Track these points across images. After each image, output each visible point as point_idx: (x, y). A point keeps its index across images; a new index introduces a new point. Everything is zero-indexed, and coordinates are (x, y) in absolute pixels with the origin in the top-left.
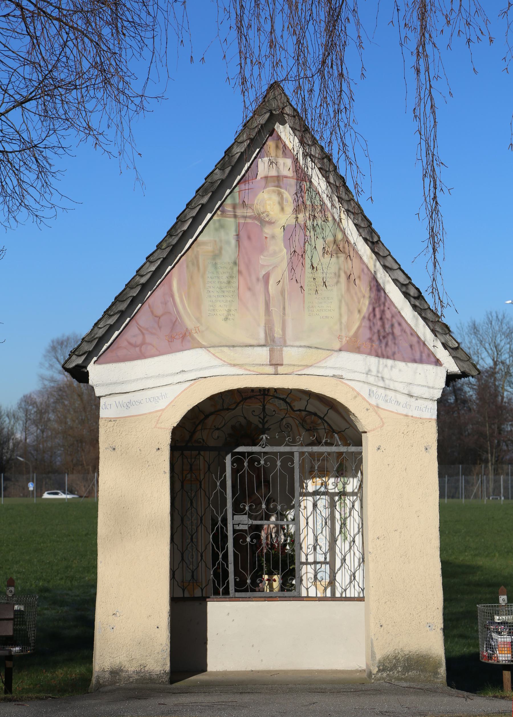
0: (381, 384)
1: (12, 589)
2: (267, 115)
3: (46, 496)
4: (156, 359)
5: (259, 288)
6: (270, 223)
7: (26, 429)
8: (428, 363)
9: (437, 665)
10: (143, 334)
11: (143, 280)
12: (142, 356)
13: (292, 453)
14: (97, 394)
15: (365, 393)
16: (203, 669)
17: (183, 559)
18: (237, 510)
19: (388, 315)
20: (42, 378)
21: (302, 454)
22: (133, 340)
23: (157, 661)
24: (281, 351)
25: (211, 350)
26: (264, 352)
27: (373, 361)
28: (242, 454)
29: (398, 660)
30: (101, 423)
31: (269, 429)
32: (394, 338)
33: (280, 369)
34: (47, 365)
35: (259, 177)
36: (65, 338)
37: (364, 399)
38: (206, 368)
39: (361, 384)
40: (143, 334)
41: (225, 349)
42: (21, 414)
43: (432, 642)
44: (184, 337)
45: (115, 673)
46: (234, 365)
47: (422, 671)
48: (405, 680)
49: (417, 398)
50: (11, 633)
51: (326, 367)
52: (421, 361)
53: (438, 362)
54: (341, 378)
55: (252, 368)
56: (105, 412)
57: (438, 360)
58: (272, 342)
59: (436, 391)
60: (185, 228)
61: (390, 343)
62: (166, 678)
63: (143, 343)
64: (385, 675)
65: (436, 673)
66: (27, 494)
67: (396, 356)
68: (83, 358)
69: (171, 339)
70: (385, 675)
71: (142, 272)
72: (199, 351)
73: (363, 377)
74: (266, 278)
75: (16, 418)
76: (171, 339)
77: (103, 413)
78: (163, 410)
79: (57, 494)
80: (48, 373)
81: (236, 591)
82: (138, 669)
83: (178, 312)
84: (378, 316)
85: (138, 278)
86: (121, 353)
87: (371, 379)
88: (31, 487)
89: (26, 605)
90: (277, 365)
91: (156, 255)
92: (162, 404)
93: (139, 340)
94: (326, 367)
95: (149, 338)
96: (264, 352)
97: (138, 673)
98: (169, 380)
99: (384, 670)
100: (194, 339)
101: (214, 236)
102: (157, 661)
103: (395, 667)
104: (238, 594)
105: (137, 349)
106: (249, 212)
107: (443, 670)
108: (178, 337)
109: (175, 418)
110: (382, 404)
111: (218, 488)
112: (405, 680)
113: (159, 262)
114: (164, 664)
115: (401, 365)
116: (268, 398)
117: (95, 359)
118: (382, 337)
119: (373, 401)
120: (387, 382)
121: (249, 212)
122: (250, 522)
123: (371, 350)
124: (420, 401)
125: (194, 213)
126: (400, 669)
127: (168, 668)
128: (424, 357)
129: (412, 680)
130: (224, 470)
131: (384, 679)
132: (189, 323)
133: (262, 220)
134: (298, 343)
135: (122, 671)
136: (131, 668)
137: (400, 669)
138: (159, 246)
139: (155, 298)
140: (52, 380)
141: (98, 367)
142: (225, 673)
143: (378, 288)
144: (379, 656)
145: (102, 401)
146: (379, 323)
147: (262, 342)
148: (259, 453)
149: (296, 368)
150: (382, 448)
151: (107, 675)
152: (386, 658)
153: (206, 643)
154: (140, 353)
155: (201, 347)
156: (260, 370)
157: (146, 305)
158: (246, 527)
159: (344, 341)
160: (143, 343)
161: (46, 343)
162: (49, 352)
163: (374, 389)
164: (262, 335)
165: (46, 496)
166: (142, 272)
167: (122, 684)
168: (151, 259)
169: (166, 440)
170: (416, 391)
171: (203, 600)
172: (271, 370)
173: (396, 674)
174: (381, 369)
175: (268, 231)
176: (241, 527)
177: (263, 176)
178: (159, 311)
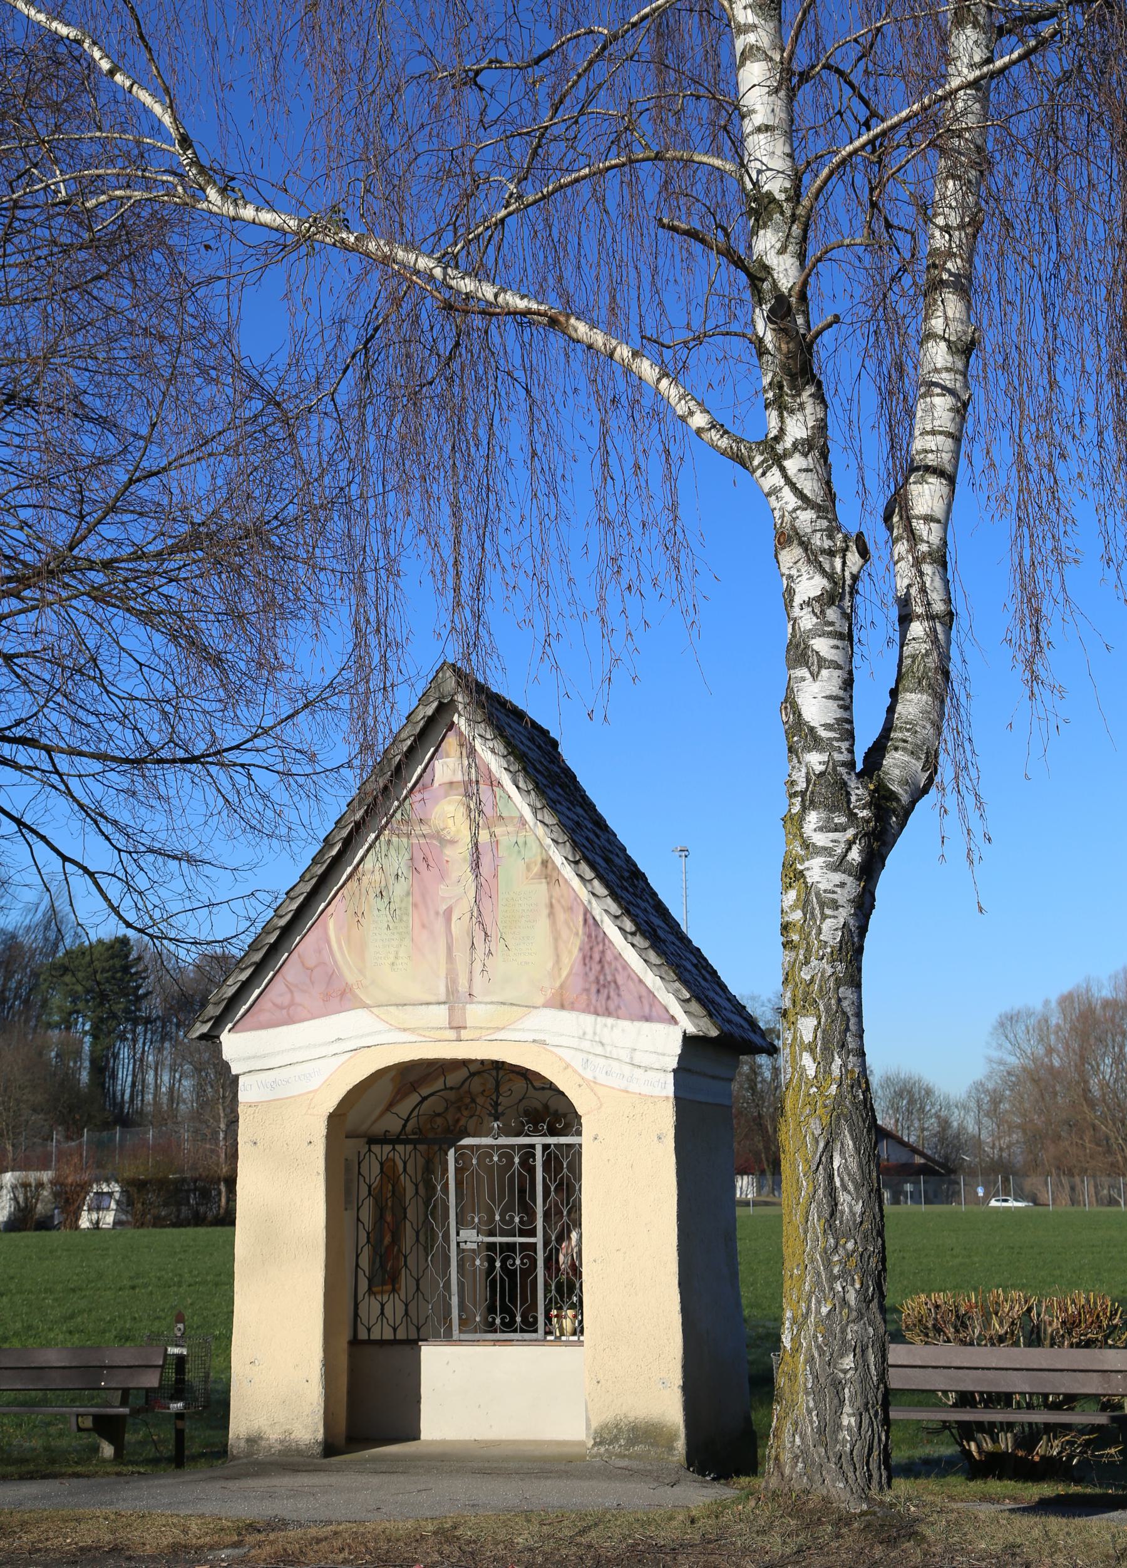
0: (599, 1050)
1: (181, 1326)
2: (435, 704)
3: (993, 1203)
4: (306, 1024)
5: (439, 925)
6: (453, 842)
7: (979, 1122)
8: (660, 1020)
9: (673, 1438)
10: (291, 992)
11: (283, 922)
12: (290, 1021)
13: (533, 1146)
14: (234, 1072)
15: (577, 1065)
16: (416, 1436)
17: (418, 1289)
18: (461, 1223)
19: (609, 956)
20: (990, 1060)
21: (546, 1147)
22: (279, 1001)
23: (306, 1427)
24: (464, 1008)
25: (375, 1010)
26: (440, 1014)
27: (588, 1020)
28: (471, 1147)
29: (620, 1430)
30: (241, 1109)
31: (503, 1114)
32: (618, 987)
33: (464, 1034)
34: (994, 1044)
35: (436, 784)
36: (1015, 1012)
37: (575, 1071)
38: (368, 1035)
39: (573, 1052)
40: (291, 992)
41: (392, 1009)
42: (973, 1105)
43: (666, 1406)
44: (343, 994)
45: (253, 1441)
46: (405, 1030)
47: (652, 1445)
48: (630, 1457)
49: (646, 1069)
50: (156, 1385)
51: (523, 1030)
52: (647, 1019)
53: (673, 1020)
54: (543, 1043)
55: (427, 1033)
56: (246, 1094)
57: (673, 1017)
58: (455, 999)
59: (667, 1059)
60: (334, 852)
61: (612, 994)
62: (318, 1450)
63: (292, 1003)
64: (602, 1449)
65: (671, 1448)
66: (977, 1201)
67: (620, 1012)
68: (210, 1024)
69: (327, 997)
70: (602, 1449)
71: (280, 912)
72: (360, 1013)
73: (574, 1043)
74: (448, 913)
75: (964, 1107)
76: (327, 997)
77: (242, 1097)
78: (315, 1091)
79: (1006, 1201)
80: (996, 1054)
81: (461, 1331)
82: (282, 1437)
83: (335, 962)
84: (597, 957)
85: (276, 920)
86: (264, 1017)
87: (586, 1045)
88: (981, 1192)
89: (189, 1347)
90: (458, 1028)
91: (297, 891)
92: (315, 1083)
93: (286, 1000)
94: (523, 1030)
95: (299, 998)
96: (443, 1010)
97: (281, 1442)
98: (323, 1051)
99: (601, 1443)
100: (355, 996)
101: (380, 863)
102: (306, 1427)
103: (616, 1439)
104: (464, 1336)
105: (284, 1012)
106: (425, 830)
107: (680, 1445)
108: (338, 996)
109: (331, 1102)
110: (602, 1078)
111: (439, 1193)
112: (630, 1457)
113: (302, 898)
114: (316, 1431)
115: (626, 1024)
116: (501, 1073)
117: (230, 1026)
118: (601, 990)
119: (588, 1075)
120: (608, 1048)
121: (425, 830)
122: (481, 1238)
123: (588, 1005)
124: (650, 1073)
125: (345, 833)
126: (622, 1442)
127: (320, 1436)
128: (649, 1012)
129: (639, 1457)
130: (446, 1170)
131: (601, 1455)
132: (350, 977)
133: (442, 840)
134: (488, 999)
135: (261, 1438)
136: (273, 1435)
137: (622, 1442)
138: (302, 877)
139: (307, 946)
140: (1001, 1062)
141: (233, 1036)
142: (443, 1442)
143: (590, 922)
144: (594, 1425)
145: (241, 1080)
146: (597, 967)
147: (443, 998)
148: (491, 1147)
149: (484, 1032)
150: (600, 1138)
151: (242, 1444)
152: (605, 1427)
153: (419, 1402)
154: (288, 1017)
155: (365, 1006)
156: (439, 1035)
157: (295, 955)
158: (474, 1246)
159: (549, 994)
160: (292, 1003)
161: (992, 1019)
162: (995, 1029)
163: (591, 1057)
164: (442, 990)
165: (993, 1203)
166: (280, 912)
167: (261, 1457)
168: (292, 894)
169: (320, 1129)
170: (639, 1058)
171: (413, 1345)
172: (452, 1034)
173: (617, 1450)
174: (598, 1031)
175: (449, 852)
176: (469, 1246)
177: (446, 780)
178: (311, 962)
